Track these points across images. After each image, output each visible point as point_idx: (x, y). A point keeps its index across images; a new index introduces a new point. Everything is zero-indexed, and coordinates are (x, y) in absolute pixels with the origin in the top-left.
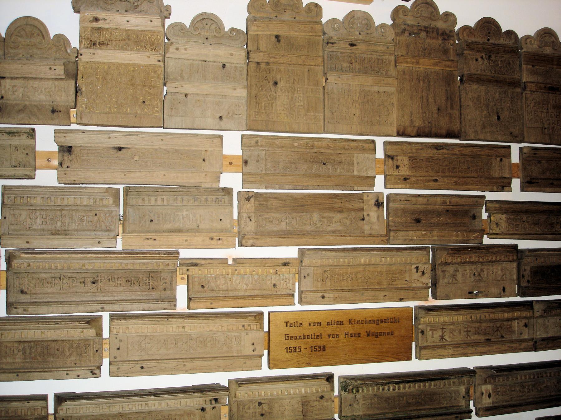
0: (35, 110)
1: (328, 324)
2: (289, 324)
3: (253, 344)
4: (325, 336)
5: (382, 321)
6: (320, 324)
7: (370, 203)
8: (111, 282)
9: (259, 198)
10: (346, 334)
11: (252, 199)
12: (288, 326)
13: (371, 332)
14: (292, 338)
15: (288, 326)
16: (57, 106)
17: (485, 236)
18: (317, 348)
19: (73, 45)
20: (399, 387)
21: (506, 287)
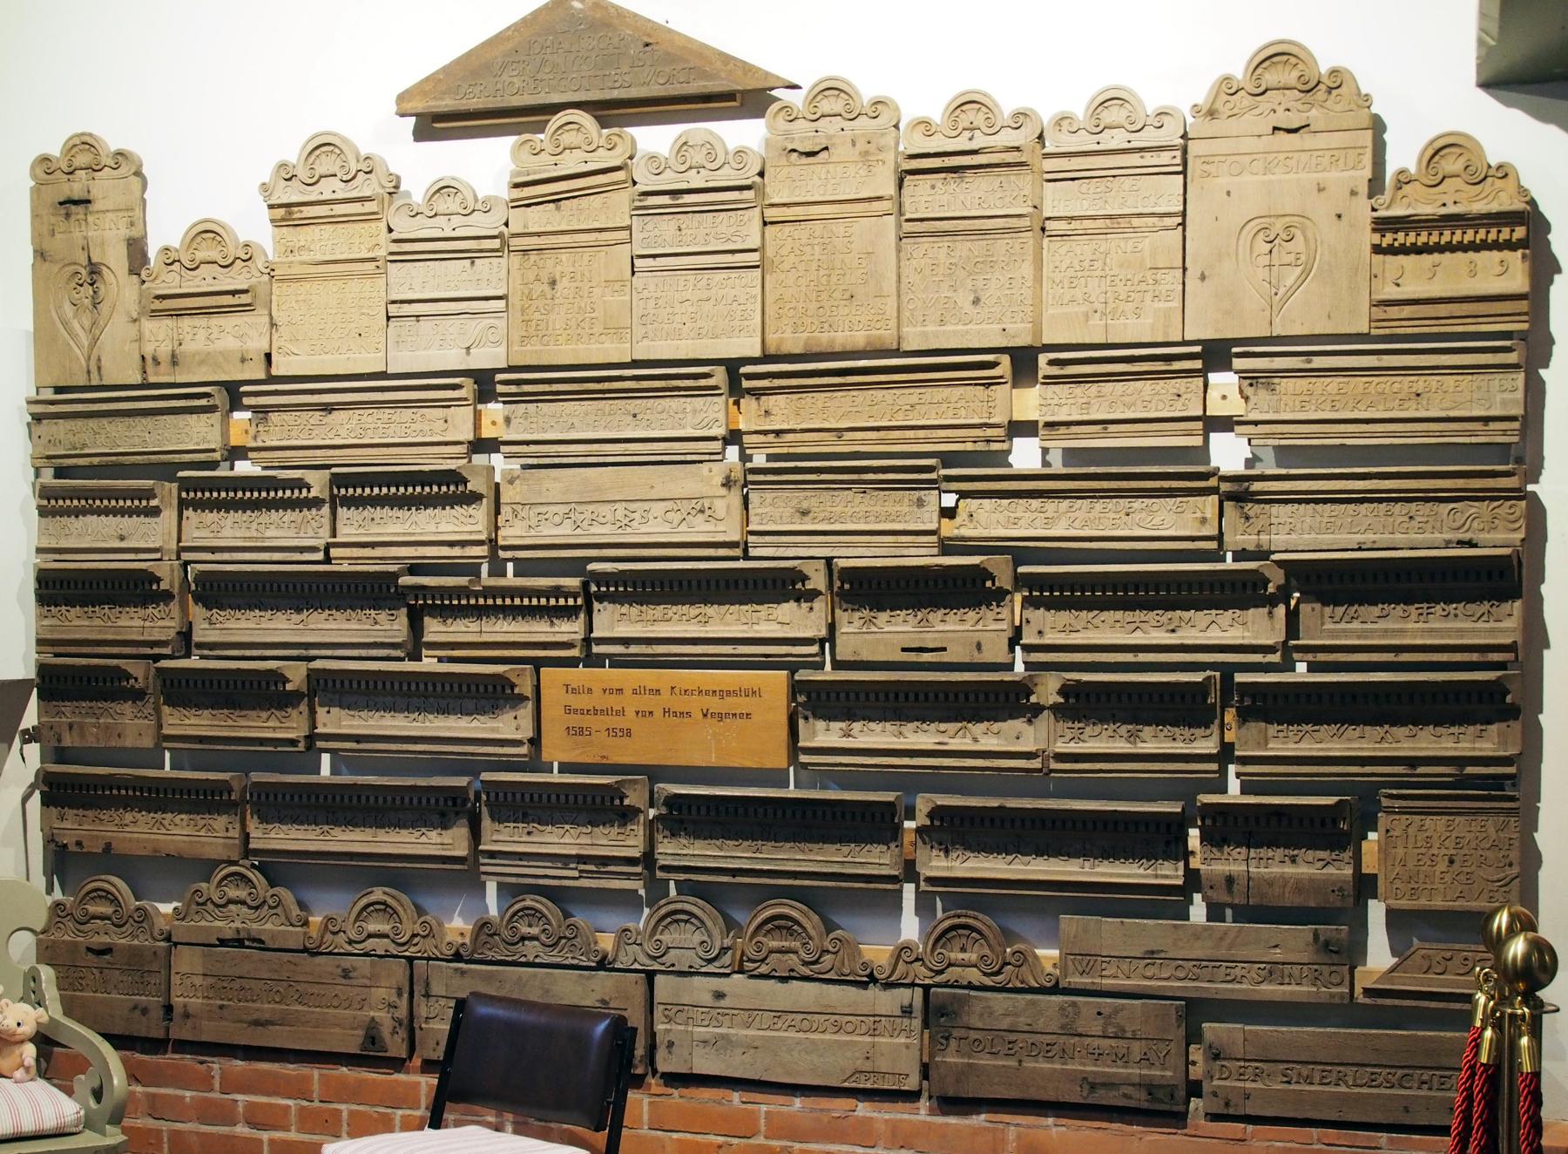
0: (221, 359)
1: (635, 692)
2: (570, 689)
3: (1563, 535)
4: (630, 712)
5: (729, 693)
6: (620, 691)
7: (714, 482)
8: (851, 239)
9: (528, 480)
10: (665, 712)
11: (517, 482)
12: (570, 691)
13: (710, 712)
14: (576, 711)
15: (570, 691)
16: (247, 351)
17: (594, 646)
18: (618, 731)
19: (283, 213)
20: (766, 811)
21: (983, 643)
